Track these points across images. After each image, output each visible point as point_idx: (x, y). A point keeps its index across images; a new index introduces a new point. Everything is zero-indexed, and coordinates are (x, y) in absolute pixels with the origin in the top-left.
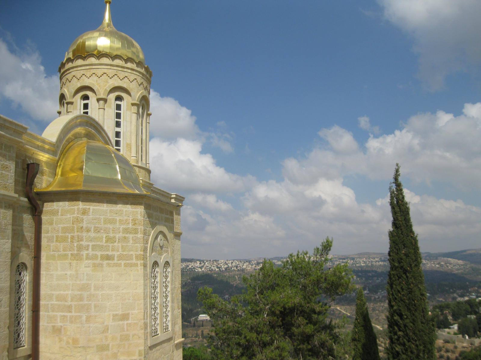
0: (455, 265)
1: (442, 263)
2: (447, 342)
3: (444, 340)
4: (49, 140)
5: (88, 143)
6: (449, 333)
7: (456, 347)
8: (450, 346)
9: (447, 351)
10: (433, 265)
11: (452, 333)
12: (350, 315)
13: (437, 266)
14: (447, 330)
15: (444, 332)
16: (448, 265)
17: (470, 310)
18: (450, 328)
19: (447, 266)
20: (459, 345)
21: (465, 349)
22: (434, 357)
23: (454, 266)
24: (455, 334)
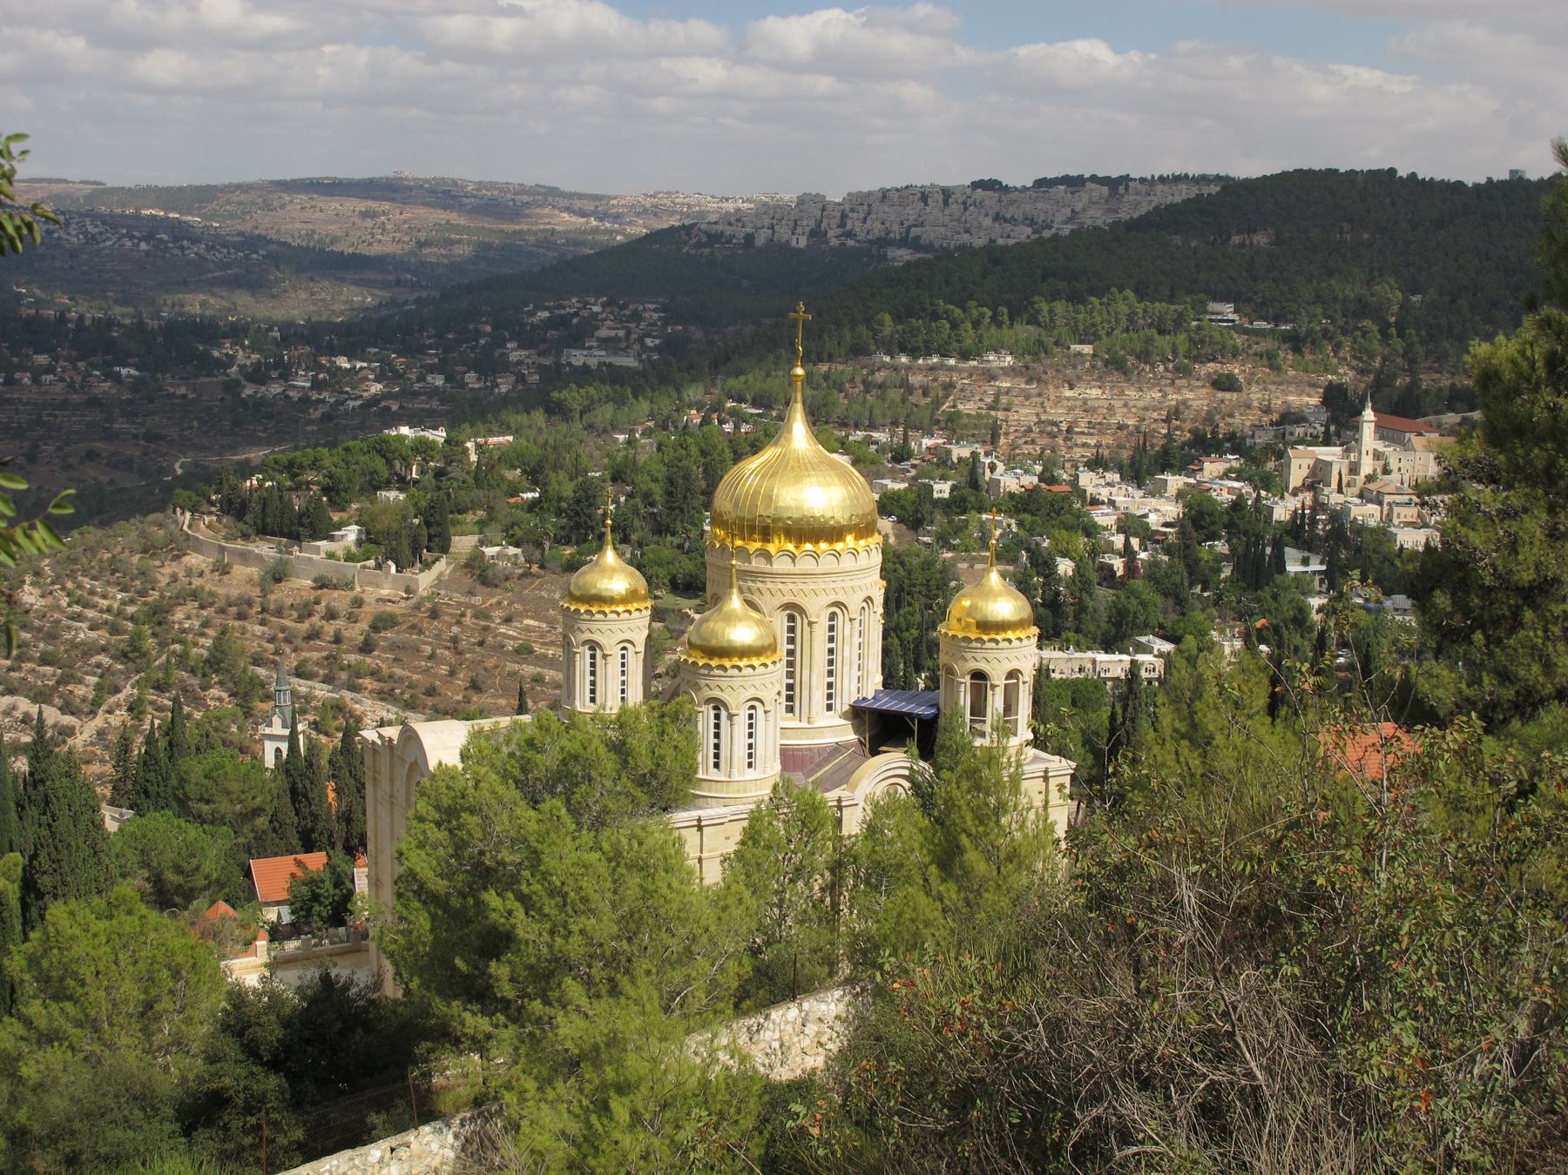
0: (213, 247)
1: (164, 237)
2: (322, 584)
3: (315, 580)
4: (598, 205)
5: (1288, 533)
6: (331, 556)
7: (358, 602)
8: (338, 599)
9: (331, 615)
10: (129, 244)
11: (340, 553)
12: (76, 489)
13: (143, 246)
14: (323, 544)
15: (317, 550)
16: (185, 243)
17: (385, 474)
18: (331, 538)
19: (182, 249)
20: (371, 594)
21: (389, 608)
22: (1286, 356)
23: (209, 248)
24: (350, 557)
